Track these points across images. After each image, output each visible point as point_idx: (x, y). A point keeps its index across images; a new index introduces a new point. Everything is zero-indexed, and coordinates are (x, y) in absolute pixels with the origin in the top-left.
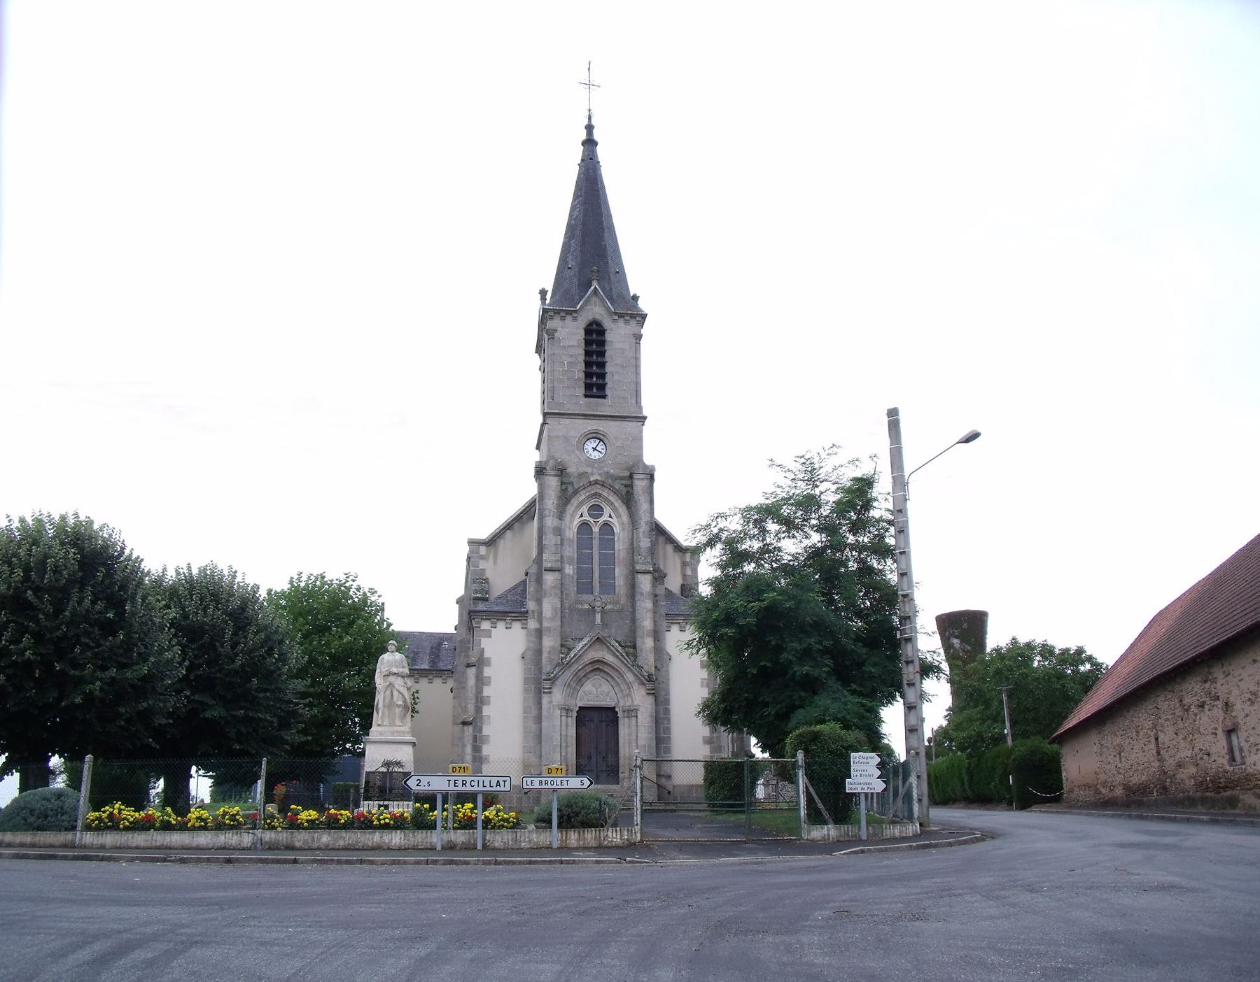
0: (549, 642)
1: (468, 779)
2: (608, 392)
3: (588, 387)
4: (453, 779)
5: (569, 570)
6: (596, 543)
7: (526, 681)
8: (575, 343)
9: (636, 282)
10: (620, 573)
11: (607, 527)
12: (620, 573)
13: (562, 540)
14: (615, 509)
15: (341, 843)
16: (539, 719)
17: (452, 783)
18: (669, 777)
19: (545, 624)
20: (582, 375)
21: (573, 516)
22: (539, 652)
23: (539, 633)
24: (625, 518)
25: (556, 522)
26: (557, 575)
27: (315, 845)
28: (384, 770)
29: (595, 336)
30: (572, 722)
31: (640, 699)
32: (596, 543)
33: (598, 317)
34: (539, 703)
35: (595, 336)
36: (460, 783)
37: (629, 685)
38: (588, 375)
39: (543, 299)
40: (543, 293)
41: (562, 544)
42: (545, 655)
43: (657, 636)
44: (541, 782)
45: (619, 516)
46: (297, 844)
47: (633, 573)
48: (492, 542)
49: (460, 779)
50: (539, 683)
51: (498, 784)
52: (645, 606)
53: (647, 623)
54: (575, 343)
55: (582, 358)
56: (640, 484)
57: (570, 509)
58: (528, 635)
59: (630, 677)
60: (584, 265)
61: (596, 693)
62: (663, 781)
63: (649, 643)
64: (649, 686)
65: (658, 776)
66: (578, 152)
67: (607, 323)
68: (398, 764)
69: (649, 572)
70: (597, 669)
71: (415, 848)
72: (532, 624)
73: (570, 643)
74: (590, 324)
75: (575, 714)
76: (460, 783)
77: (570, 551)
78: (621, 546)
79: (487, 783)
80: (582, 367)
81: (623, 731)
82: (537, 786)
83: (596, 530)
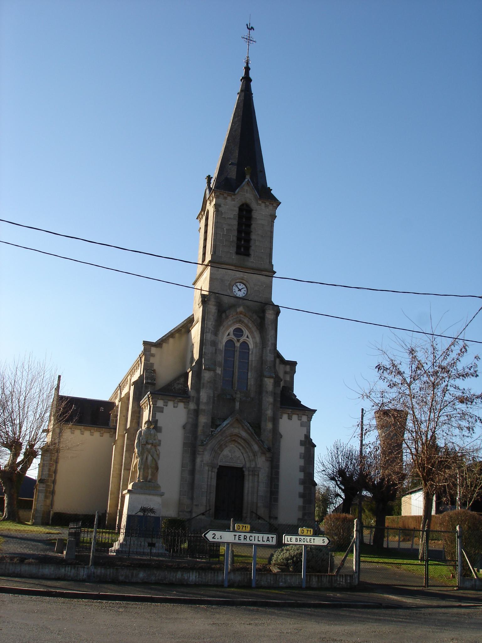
0: (203, 420)
1: (248, 535)
2: (252, 252)
3: (238, 247)
4: (238, 534)
5: (219, 371)
6: (237, 354)
7: (185, 444)
8: (232, 216)
9: (274, 181)
10: (251, 375)
11: (245, 344)
12: (251, 375)
13: (216, 350)
14: (251, 332)
15: (153, 578)
16: (193, 472)
17: (237, 537)
18: (276, 518)
19: (202, 407)
20: (235, 239)
21: (223, 334)
22: (195, 425)
23: (197, 413)
24: (258, 339)
25: (213, 338)
26: (212, 373)
27: (134, 580)
28: (141, 514)
29: (245, 214)
30: (214, 475)
31: (262, 462)
32: (237, 354)
33: (248, 201)
34: (193, 461)
35: (245, 214)
36: (242, 538)
37: (255, 454)
38: (239, 239)
39: (209, 183)
40: (209, 178)
41: (216, 353)
42: (200, 429)
43: (275, 420)
44: (296, 539)
45: (253, 337)
46: (121, 578)
47: (260, 376)
48: (159, 344)
49: (243, 534)
50: (192, 446)
51: (268, 540)
52: (268, 400)
53: (269, 413)
54: (232, 216)
55: (236, 227)
56: (269, 315)
57: (222, 329)
58: (188, 413)
59: (256, 447)
60: (240, 165)
61: (233, 455)
62: (272, 521)
63: (270, 426)
64: (268, 455)
65: (270, 517)
66: (238, 86)
67: (254, 206)
68: (152, 510)
69: (272, 377)
70: (234, 440)
71: (207, 585)
72: (192, 406)
73: (218, 422)
74: (243, 205)
75: (216, 470)
76: (242, 538)
77: (220, 358)
78: (253, 358)
79: (260, 539)
80: (235, 233)
81: (248, 485)
82: (294, 542)
83: (238, 345)
